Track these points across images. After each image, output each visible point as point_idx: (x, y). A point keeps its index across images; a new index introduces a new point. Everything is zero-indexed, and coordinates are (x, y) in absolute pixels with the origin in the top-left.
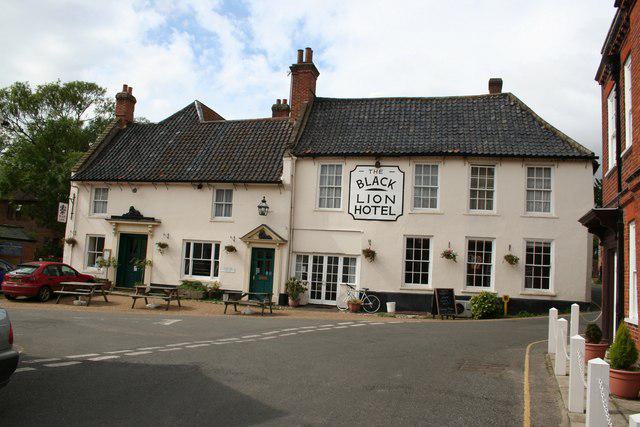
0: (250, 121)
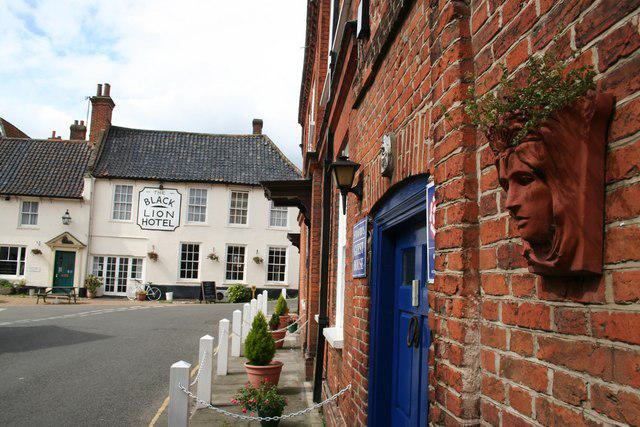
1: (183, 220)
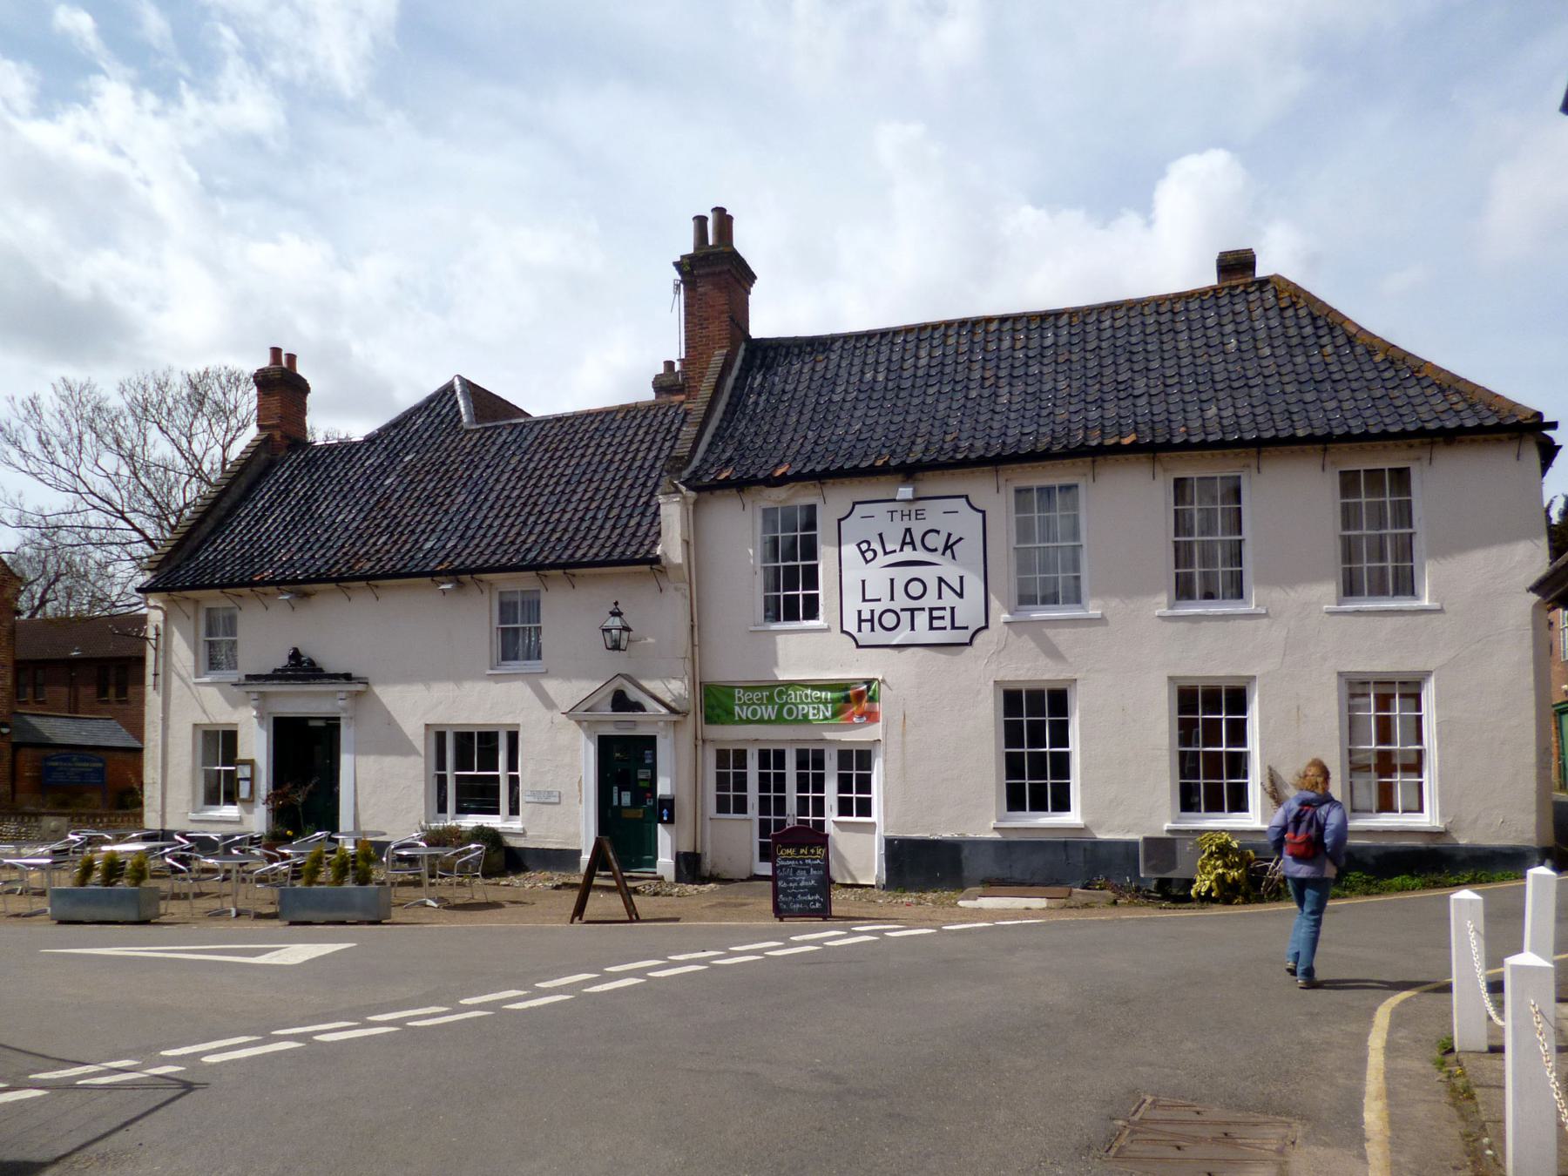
0: (588, 414)
1: (1000, 615)
